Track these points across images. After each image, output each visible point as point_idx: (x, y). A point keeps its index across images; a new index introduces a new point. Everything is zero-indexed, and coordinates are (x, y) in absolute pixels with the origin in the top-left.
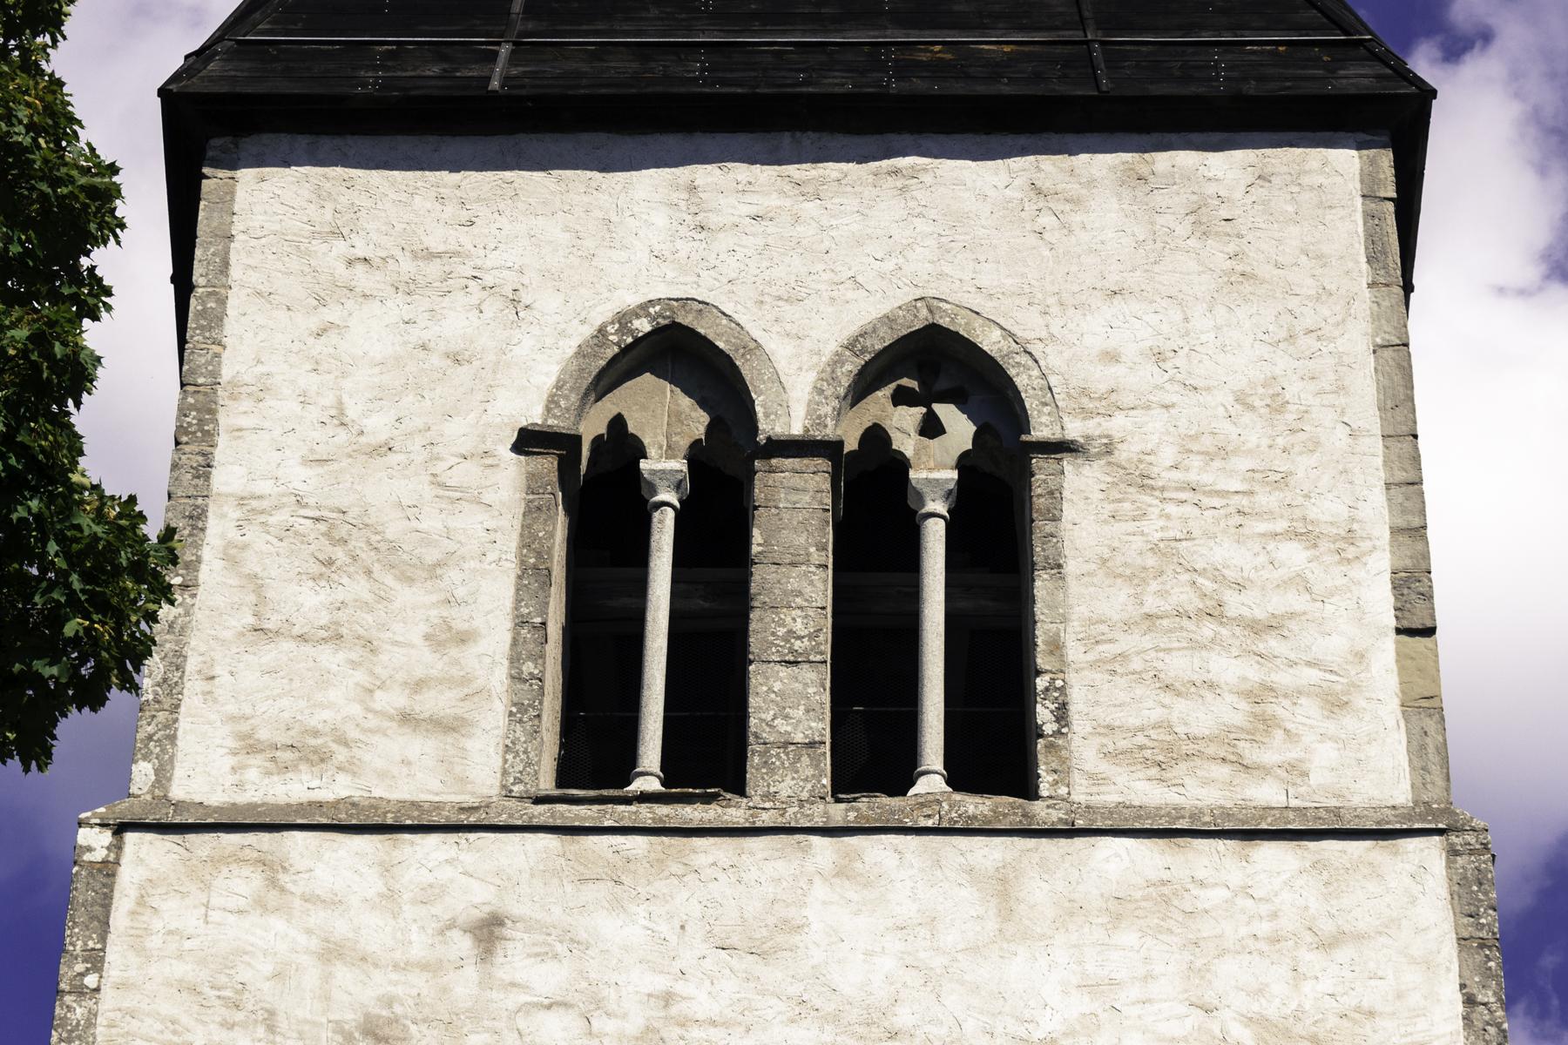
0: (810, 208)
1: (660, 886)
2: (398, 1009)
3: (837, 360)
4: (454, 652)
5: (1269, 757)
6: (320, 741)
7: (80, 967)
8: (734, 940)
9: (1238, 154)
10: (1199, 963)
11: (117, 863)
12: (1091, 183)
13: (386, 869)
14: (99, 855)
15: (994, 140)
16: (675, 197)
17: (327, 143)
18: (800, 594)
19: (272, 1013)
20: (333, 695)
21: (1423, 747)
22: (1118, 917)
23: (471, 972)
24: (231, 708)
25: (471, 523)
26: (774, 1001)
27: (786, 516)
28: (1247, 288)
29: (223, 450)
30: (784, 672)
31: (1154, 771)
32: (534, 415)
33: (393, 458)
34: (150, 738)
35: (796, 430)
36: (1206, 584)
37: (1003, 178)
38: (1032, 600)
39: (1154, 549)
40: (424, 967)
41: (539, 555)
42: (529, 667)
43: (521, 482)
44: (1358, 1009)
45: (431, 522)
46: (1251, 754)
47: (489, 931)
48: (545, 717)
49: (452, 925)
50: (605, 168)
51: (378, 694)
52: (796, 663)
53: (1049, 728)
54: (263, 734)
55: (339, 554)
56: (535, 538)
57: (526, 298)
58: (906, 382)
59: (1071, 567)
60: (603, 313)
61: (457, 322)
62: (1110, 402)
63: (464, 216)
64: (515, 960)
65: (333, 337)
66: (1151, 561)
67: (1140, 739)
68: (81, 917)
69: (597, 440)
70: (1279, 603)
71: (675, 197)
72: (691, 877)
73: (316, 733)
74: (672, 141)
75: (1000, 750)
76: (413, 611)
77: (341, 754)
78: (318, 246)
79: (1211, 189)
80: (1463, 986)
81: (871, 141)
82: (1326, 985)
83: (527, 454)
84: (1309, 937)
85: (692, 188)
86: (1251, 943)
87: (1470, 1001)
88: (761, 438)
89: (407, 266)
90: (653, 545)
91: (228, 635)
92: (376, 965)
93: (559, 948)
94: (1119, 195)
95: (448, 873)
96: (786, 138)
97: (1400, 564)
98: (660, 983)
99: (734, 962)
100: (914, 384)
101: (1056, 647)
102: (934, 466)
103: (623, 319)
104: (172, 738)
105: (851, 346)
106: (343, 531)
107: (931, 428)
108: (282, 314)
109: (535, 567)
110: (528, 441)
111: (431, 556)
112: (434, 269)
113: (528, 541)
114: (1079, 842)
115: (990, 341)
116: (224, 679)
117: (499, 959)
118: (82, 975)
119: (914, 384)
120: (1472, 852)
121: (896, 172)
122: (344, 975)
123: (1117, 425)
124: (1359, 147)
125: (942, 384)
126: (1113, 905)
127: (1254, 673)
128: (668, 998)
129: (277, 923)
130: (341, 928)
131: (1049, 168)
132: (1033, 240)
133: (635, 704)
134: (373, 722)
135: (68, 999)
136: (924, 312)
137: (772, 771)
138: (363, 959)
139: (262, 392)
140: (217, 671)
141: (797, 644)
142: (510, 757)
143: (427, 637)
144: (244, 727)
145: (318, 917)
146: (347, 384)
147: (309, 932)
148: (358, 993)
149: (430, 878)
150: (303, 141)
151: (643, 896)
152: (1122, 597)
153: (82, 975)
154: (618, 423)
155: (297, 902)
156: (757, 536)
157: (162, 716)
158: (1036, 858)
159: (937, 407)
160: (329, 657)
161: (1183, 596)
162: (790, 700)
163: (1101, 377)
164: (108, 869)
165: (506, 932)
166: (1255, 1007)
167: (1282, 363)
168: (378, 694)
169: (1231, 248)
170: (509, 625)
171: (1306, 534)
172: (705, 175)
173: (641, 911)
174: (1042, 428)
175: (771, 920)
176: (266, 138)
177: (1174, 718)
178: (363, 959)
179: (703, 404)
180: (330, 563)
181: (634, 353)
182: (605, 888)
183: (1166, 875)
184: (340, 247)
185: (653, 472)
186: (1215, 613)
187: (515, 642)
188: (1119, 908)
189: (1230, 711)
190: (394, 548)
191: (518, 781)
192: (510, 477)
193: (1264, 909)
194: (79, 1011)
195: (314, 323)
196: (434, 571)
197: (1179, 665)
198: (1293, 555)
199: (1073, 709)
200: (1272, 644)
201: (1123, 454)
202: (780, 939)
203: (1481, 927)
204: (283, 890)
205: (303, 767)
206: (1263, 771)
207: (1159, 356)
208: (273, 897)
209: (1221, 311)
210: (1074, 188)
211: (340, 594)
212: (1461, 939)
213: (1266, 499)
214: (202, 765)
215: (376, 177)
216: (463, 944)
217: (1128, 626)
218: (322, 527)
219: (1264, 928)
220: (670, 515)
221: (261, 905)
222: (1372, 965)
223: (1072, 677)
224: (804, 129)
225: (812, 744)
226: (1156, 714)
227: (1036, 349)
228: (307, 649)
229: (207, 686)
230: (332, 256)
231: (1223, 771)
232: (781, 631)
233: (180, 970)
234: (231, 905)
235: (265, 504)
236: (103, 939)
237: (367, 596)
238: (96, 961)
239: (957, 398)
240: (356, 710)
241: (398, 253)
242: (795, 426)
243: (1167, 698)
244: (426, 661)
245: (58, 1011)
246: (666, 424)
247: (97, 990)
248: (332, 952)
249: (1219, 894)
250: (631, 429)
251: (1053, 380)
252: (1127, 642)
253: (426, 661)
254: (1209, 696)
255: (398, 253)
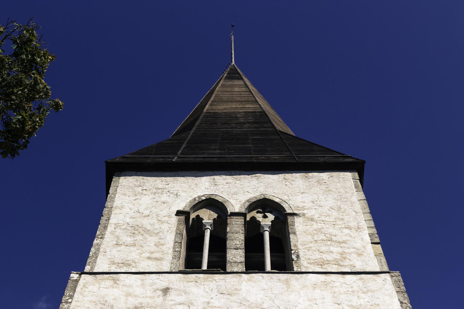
0: (238, 182)
1: (206, 283)
2: (143, 305)
3: (245, 203)
4: (160, 247)
5: (345, 264)
6: (129, 262)
7: (67, 298)
8: (224, 292)
9: (326, 173)
10: (335, 296)
11: (79, 280)
12: (296, 177)
13: (142, 280)
14: (75, 278)
15: (276, 172)
16: (210, 180)
17: (139, 173)
18: (238, 238)
19: (112, 306)
20: (133, 254)
21: (381, 262)
22: (315, 288)
23: (161, 298)
24: (110, 257)
25: (165, 227)
26: (234, 303)
27: (234, 225)
28: (330, 192)
29: (112, 216)
30: (234, 250)
31: (320, 266)
32: (181, 209)
33: (149, 217)
34: (90, 262)
35: (237, 211)
36: (328, 236)
37: (278, 177)
38: (290, 238)
39: (316, 230)
40: (151, 297)
41: (180, 231)
42: (177, 249)
43: (177, 220)
44: (375, 304)
45: (157, 226)
46: (341, 263)
47: (166, 291)
48: (182, 243)
49: (158, 289)
50: (196, 176)
51: (143, 254)
52: (237, 249)
53: (295, 259)
54: (116, 261)
55: (136, 232)
56: (180, 228)
57: (179, 194)
58: (259, 210)
59: (298, 233)
60: (195, 196)
61: (164, 198)
62: (303, 208)
63: (167, 183)
64: (172, 296)
65: (138, 200)
66: (315, 232)
67: (316, 261)
68: (69, 289)
69: (193, 219)
70: (344, 238)
71: (210, 180)
72: (214, 281)
73: (128, 261)
74: (210, 172)
75: (284, 263)
76: (152, 240)
77: (134, 264)
78: (136, 188)
79: (321, 178)
80: (399, 300)
81: (250, 172)
82: (366, 300)
83: (178, 216)
84: (361, 291)
85: (214, 179)
86: (347, 292)
87: (401, 303)
88: (229, 212)
89: (154, 190)
90: (205, 235)
91: (110, 245)
92: (139, 297)
93: (182, 294)
94: (302, 180)
95: (157, 280)
96: (233, 172)
97: (370, 232)
98: (207, 300)
99: (224, 297)
100: (261, 210)
101: (295, 246)
102: (267, 221)
103: (199, 197)
104: (95, 262)
105: (248, 201)
106: (137, 228)
107: (265, 217)
108: (128, 197)
109: (179, 233)
110: (179, 213)
111: (156, 231)
112: (160, 191)
113: (178, 229)
114: (304, 275)
115: (277, 200)
116: (108, 252)
117: (168, 295)
118: (68, 299)
119: (261, 210)
120: (396, 276)
121: (256, 176)
122: (130, 299)
123: (305, 212)
124: (350, 172)
125: (267, 210)
126: (314, 286)
127: (340, 250)
128: (208, 303)
129: (115, 290)
130: (130, 290)
131: (288, 176)
132: (285, 186)
133: (201, 246)
134: (141, 259)
135: (63, 304)
136: (263, 196)
137: (232, 267)
138: (136, 296)
139: (122, 207)
140: (107, 251)
141: (238, 246)
142: (172, 265)
143: (155, 245)
144: (112, 260)
145: (125, 289)
146: (141, 207)
147: (123, 291)
148: (133, 302)
149: (153, 281)
150: (134, 173)
151: (203, 284)
152: (310, 238)
153: (68, 299)
154: (198, 216)
155: (121, 286)
156: (228, 229)
157: (93, 258)
158: (294, 277)
159: (266, 214)
160: (132, 248)
161: (322, 237)
162: (236, 255)
163: (301, 205)
164: (77, 281)
165: (169, 291)
166: (350, 304)
167: (339, 203)
168: (143, 254)
169: (326, 187)
170: (173, 242)
171: (349, 228)
172: (217, 177)
173: (202, 287)
174: (288, 211)
175: (233, 289)
176: (127, 172)
177: (323, 257)
178: (136, 296)
179: (216, 213)
180: (134, 233)
181: (202, 204)
182: (193, 283)
183: (325, 280)
184: (141, 188)
185: (205, 223)
186: (331, 240)
187: (174, 245)
188: (315, 286)
189: (336, 256)
190: (148, 230)
191: (174, 269)
192: (174, 220)
193: (349, 286)
194: (66, 306)
195: (134, 198)
196: (157, 234)
197: (323, 249)
198: (347, 231)
199: (300, 256)
200: (344, 245)
201: (307, 216)
202: (235, 292)
203: (401, 289)
204: (118, 284)
205: (125, 267)
206: (346, 266)
207: (313, 202)
208: (115, 285)
209: (325, 196)
210: (293, 178)
211: (136, 238)
212: (397, 292)
213: (338, 222)
214: (101, 265)
215: (149, 178)
216: (160, 293)
217: (311, 242)
218: (133, 228)
219: (350, 290)
220: (209, 231)
221: (112, 287)
222: (377, 296)
223: (299, 251)
224: (237, 170)
225: (241, 262)
226: (319, 257)
227: (287, 201)
228: (128, 247)
229: (104, 254)
230: (140, 189)
231: (337, 266)
232: (234, 244)
233: (94, 299)
234: (105, 287)
235: (120, 225)
236: (74, 293)
237: (142, 239)
238: (71, 297)
239: (271, 212)
240: (138, 257)
241: (152, 189)
242: (237, 209)
243: (322, 254)
244: (153, 248)
245: (61, 306)
246: (208, 217)
247: (71, 302)
248: (128, 295)
249: (338, 284)
250: (201, 217)
251: (291, 206)
252: (311, 245)
253: (153, 248)
254: (331, 254)
255: (152, 189)
